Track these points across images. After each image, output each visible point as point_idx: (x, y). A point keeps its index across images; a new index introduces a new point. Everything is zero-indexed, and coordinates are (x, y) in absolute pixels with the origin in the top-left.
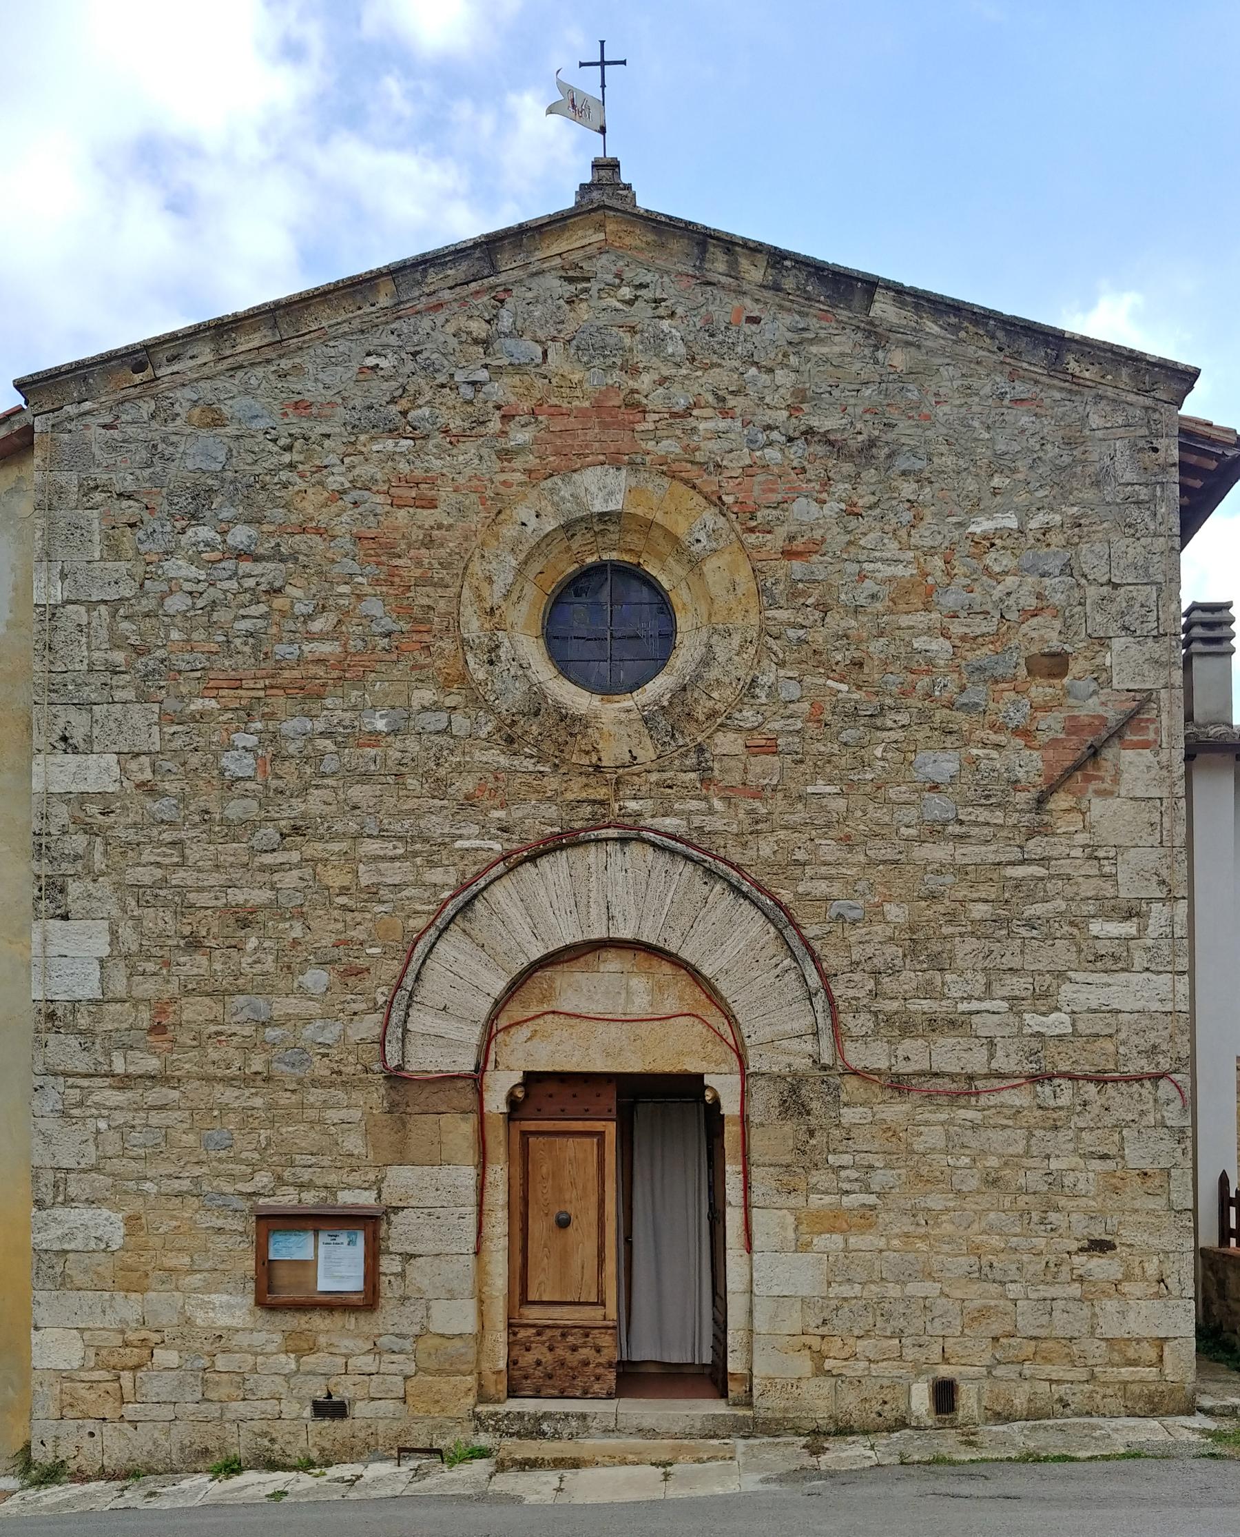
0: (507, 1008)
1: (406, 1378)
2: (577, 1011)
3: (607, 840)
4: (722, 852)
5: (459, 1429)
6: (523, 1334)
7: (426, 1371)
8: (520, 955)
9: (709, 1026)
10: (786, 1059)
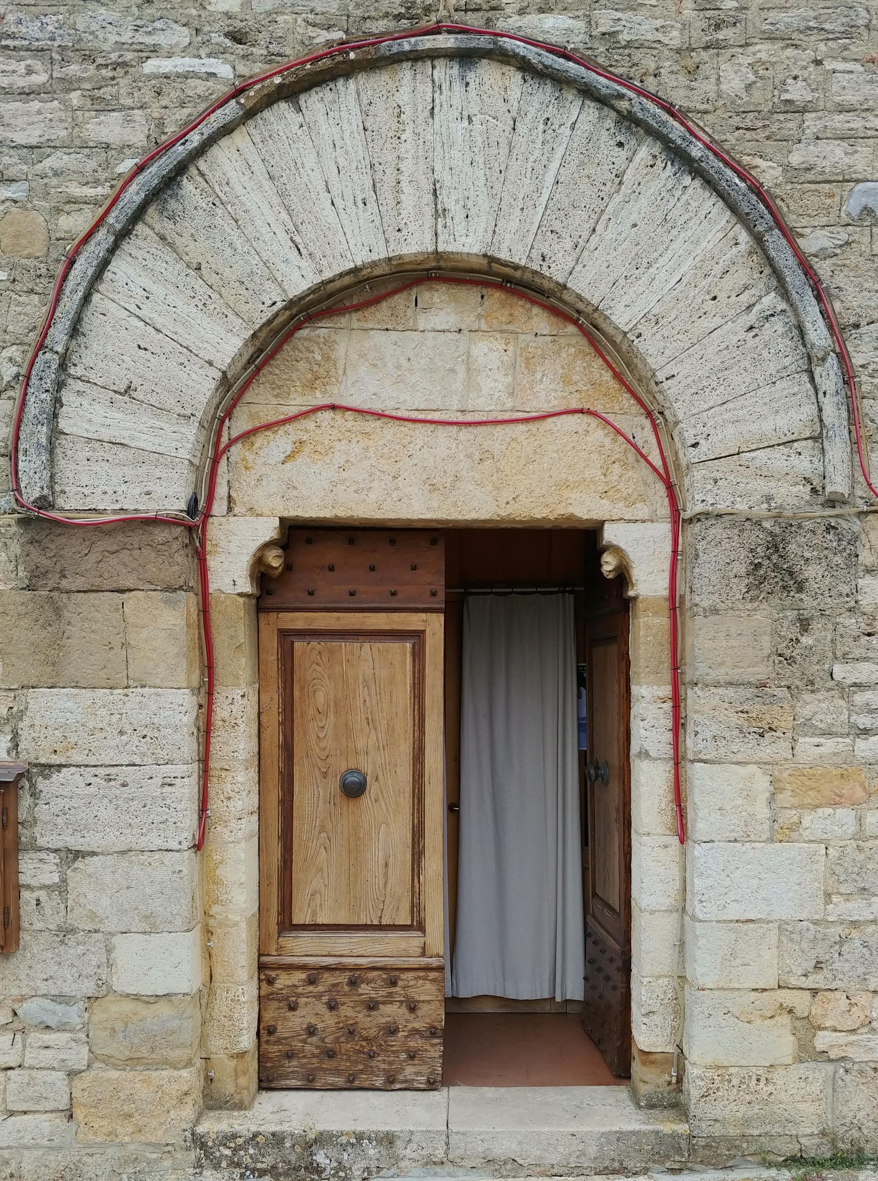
0: (248, 397)
1: (72, 1074)
2: (377, 406)
3: (433, 55)
4: (651, 84)
5: (167, 1163)
6: (284, 980)
7: (108, 1061)
8: (268, 285)
9: (618, 432)
10: (762, 487)
